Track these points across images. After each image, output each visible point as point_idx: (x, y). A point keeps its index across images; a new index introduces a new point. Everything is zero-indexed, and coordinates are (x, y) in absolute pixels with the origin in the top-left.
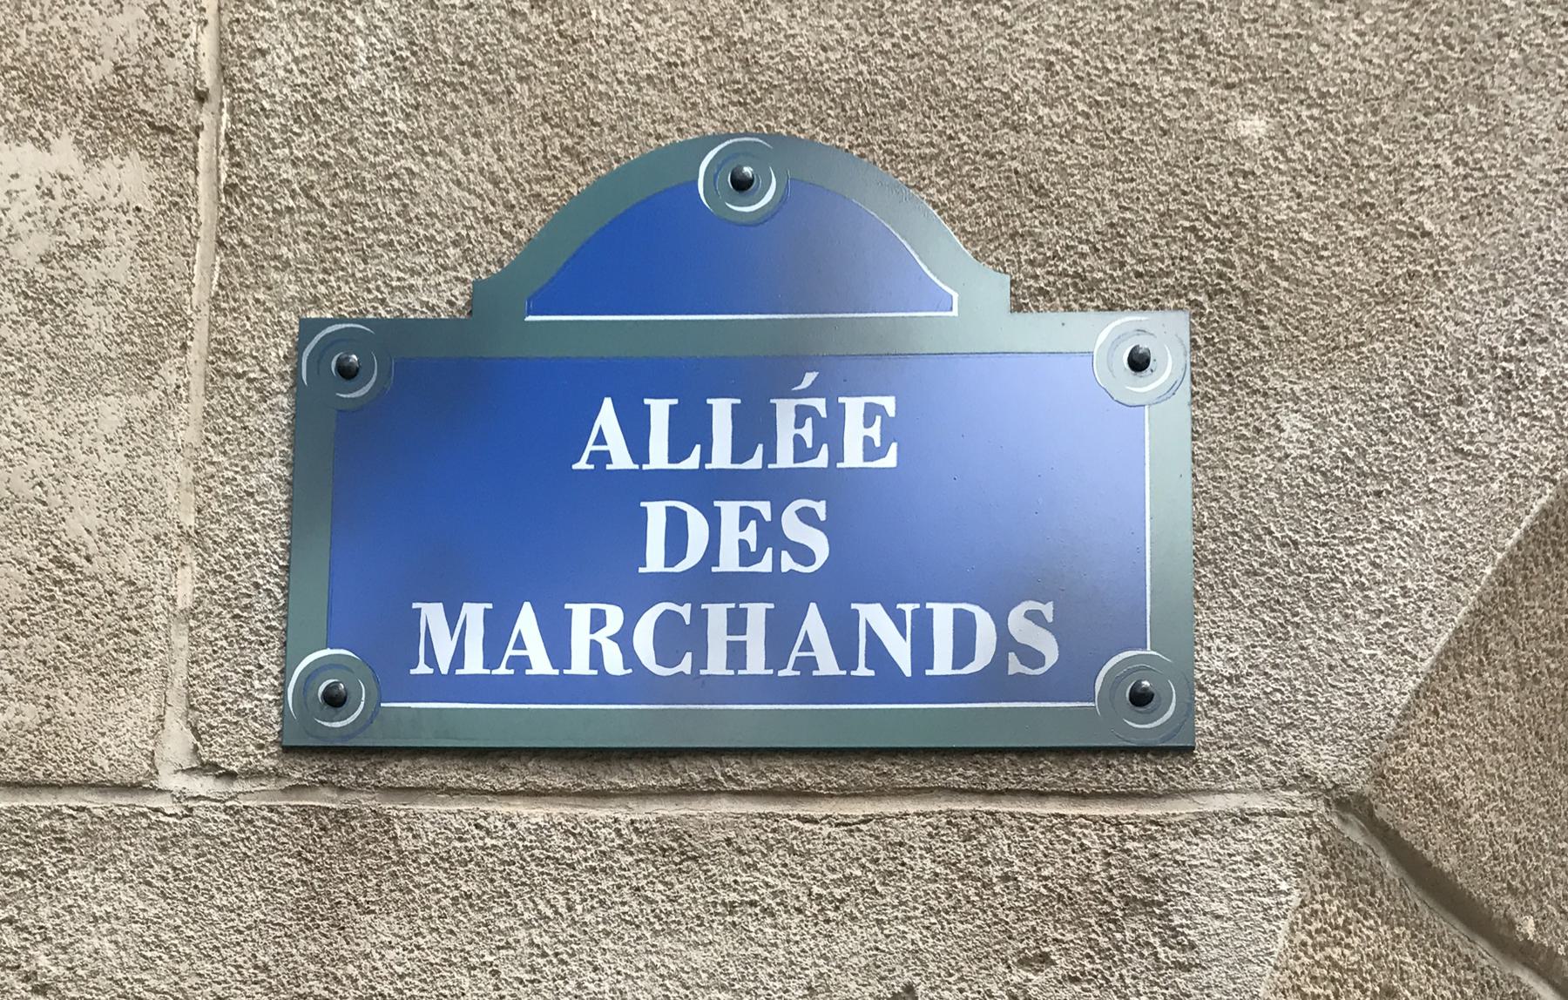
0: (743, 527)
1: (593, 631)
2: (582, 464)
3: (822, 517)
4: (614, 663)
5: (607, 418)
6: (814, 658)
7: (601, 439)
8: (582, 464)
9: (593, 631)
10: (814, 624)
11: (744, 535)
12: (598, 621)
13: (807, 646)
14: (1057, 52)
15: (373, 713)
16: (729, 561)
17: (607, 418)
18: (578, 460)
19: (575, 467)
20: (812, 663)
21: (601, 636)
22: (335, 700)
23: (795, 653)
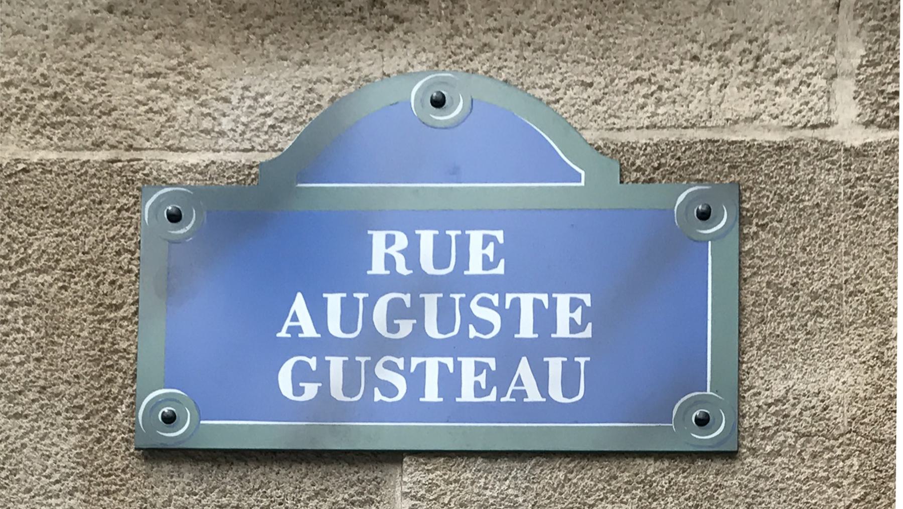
0: (484, 247)
1: (387, 247)
2: (283, 334)
3: (503, 400)
4: (402, 268)
5: (299, 305)
6: (525, 391)
7: (295, 318)
8: (283, 334)
9: (387, 247)
10: (524, 369)
11: (486, 251)
12: (390, 241)
13: (520, 382)
14: (868, 271)
15: (195, 426)
16: (475, 268)
17: (299, 305)
18: (280, 331)
19: (279, 335)
20: (524, 394)
21: (392, 251)
22: (170, 419)
23: (512, 387)
